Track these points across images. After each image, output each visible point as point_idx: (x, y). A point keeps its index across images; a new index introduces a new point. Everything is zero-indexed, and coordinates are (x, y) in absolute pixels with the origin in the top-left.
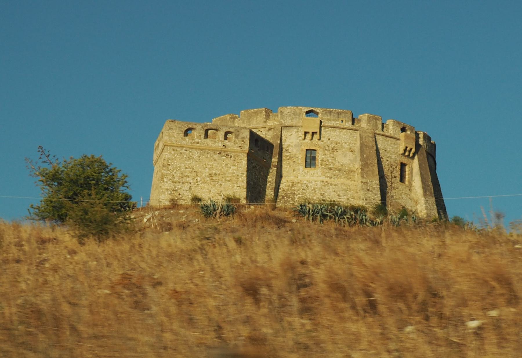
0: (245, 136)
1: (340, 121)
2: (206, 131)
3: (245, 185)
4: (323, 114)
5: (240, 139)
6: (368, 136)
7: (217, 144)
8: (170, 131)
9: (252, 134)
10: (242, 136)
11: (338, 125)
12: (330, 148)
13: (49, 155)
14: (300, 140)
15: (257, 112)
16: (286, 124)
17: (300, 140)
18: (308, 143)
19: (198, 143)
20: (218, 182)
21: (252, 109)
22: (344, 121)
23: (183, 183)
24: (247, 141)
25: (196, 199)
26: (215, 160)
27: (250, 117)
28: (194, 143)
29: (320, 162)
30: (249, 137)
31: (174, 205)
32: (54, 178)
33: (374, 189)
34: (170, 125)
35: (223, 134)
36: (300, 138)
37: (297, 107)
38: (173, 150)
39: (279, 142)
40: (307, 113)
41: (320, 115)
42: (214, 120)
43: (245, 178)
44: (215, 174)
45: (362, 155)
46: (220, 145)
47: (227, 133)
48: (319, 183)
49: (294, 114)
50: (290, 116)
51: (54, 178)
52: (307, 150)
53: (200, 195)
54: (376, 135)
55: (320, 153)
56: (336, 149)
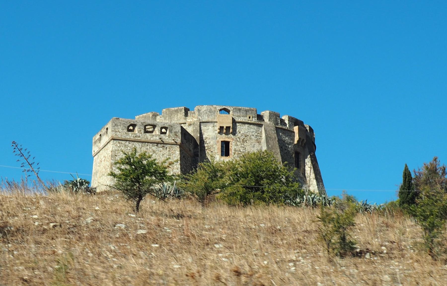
0: (177, 131)
1: (248, 117)
4: (233, 112)
5: (173, 134)
6: (271, 130)
7: (154, 137)
8: (116, 127)
10: (175, 131)
11: (247, 121)
12: (241, 140)
13: (21, 149)
14: (216, 134)
15: (177, 110)
16: (204, 120)
17: (216, 134)
18: (224, 138)
19: (139, 137)
21: (172, 107)
27: (171, 114)
28: (136, 137)
29: (233, 151)
30: (180, 131)
34: (115, 122)
35: (160, 129)
37: (212, 106)
38: (119, 143)
39: (199, 135)
40: (220, 110)
41: (231, 112)
42: (137, 117)
43: (179, 166)
46: (157, 138)
49: (210, 112)
50: (206, 113)
52: (222, 141)
56: (246, 141)
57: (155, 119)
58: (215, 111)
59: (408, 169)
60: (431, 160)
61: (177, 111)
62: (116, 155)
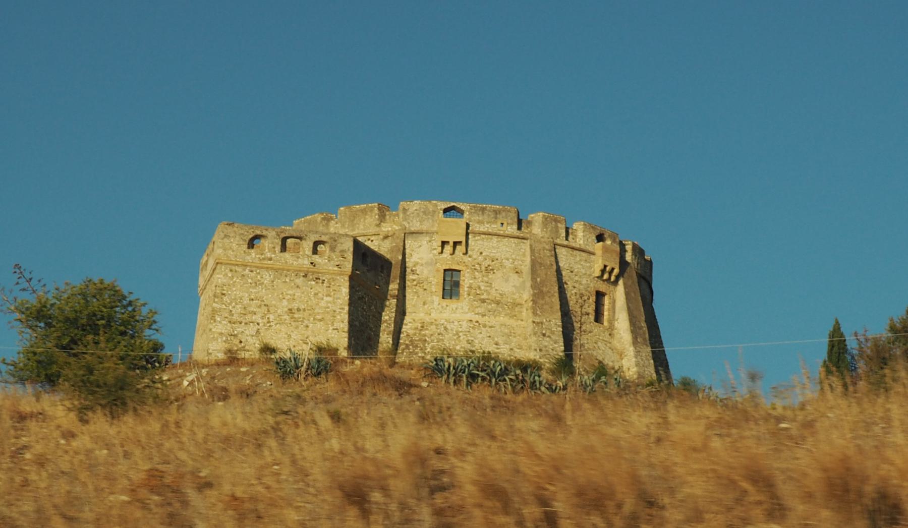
1: (499, 224)
2: (284, 240)
3: (345, 326)
4: (471, 213)
5: (337, 253)
6: (544, 249)
8: (226, 240)
9: (357, 245)
10: (341, 248)
11: (495, 231)
12: (483, 268)
13: (31, 279)
14: (434, 255)
16: (413, 229)
17: (434, 255)
18: (447, 260)
19: (270, 259)
20: (302, 322)
21: (356, 204)
22: (505, 225)
23: (246, 324)
24: (350, 256)
25: (268, 349)
26: (298, 287)
28: (264, 259)
29: (466, 289)
30: (352, 249)
31: (232, 359)
32: (39, 315)
33: (553, 333)
35: (311, 245)
36: (435, 252)
37: (430, 201)
38: (231, 270)
39: (400, 258)
40: (446, 211)
41: (466, 215)
42: (296, 222)
43: (347, 316)
44: (299, 310)
45: (533, 279)
47: (316, 244)
48: (465, 324)
49: (424, 213)
51: (39, 315)
52: (445, 270)
53: (273, 343)
54: (557, 247)
55: (467, 275)
56: (493, 270)
57: (327, 225)
58: (434, 212)
59: (839, 328)
60: (888, 322)
61: (364, 211)
62: (223, 294)
